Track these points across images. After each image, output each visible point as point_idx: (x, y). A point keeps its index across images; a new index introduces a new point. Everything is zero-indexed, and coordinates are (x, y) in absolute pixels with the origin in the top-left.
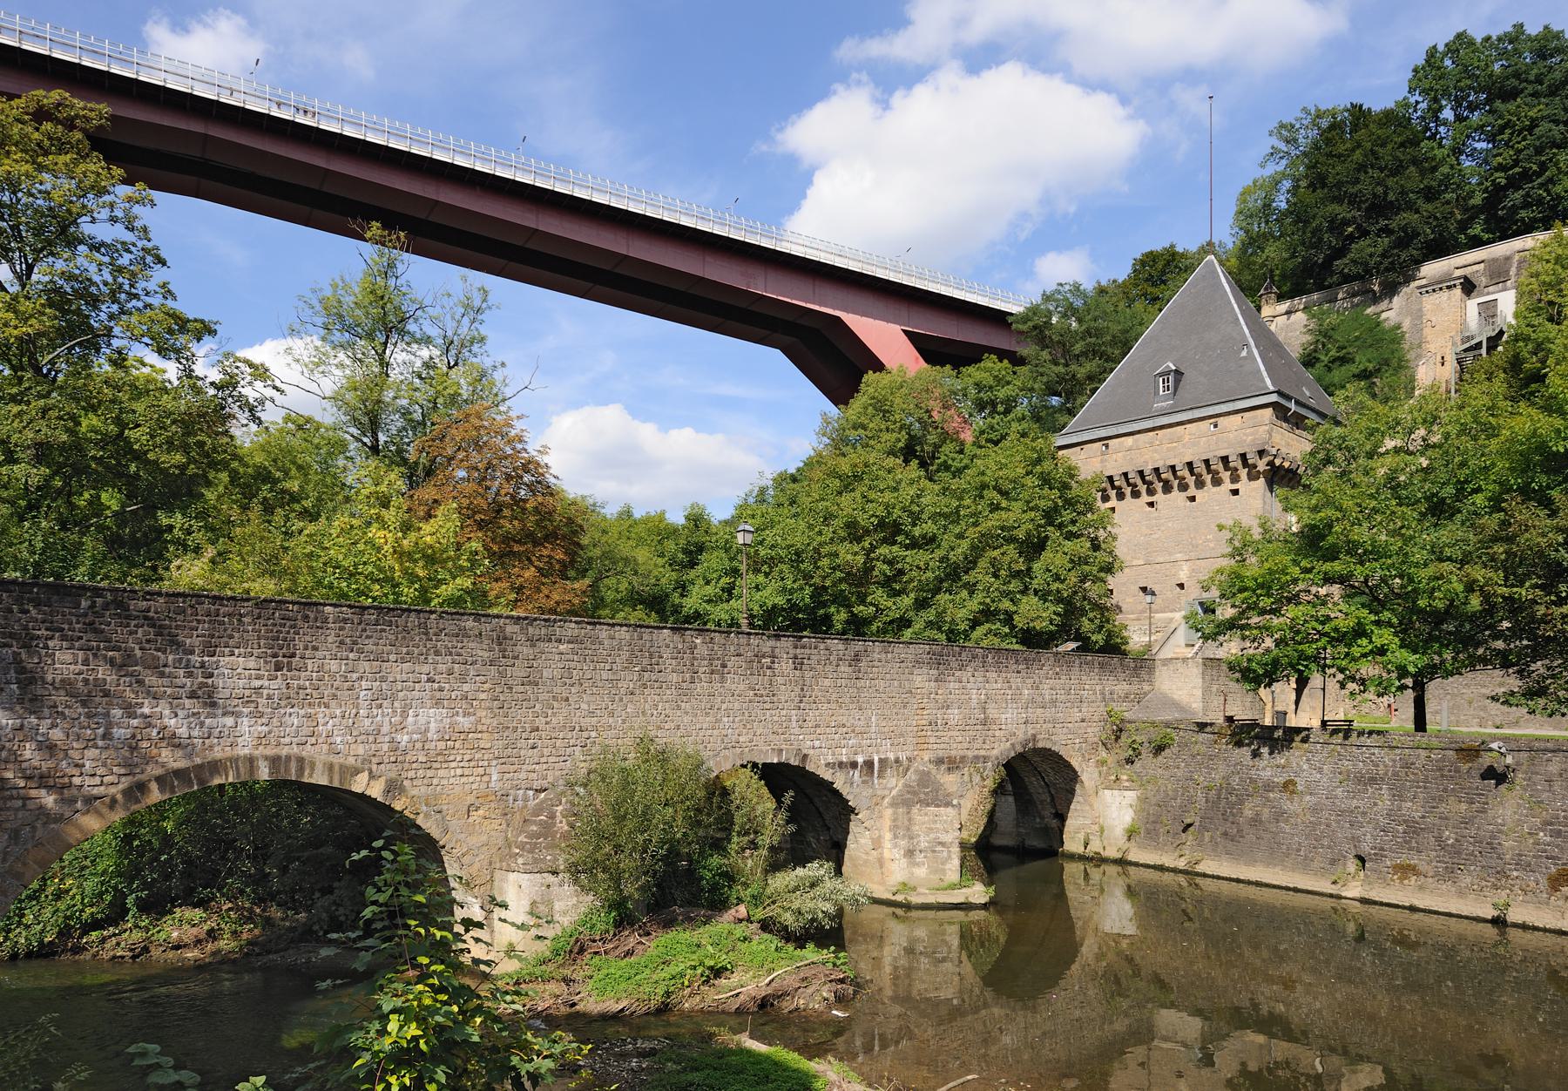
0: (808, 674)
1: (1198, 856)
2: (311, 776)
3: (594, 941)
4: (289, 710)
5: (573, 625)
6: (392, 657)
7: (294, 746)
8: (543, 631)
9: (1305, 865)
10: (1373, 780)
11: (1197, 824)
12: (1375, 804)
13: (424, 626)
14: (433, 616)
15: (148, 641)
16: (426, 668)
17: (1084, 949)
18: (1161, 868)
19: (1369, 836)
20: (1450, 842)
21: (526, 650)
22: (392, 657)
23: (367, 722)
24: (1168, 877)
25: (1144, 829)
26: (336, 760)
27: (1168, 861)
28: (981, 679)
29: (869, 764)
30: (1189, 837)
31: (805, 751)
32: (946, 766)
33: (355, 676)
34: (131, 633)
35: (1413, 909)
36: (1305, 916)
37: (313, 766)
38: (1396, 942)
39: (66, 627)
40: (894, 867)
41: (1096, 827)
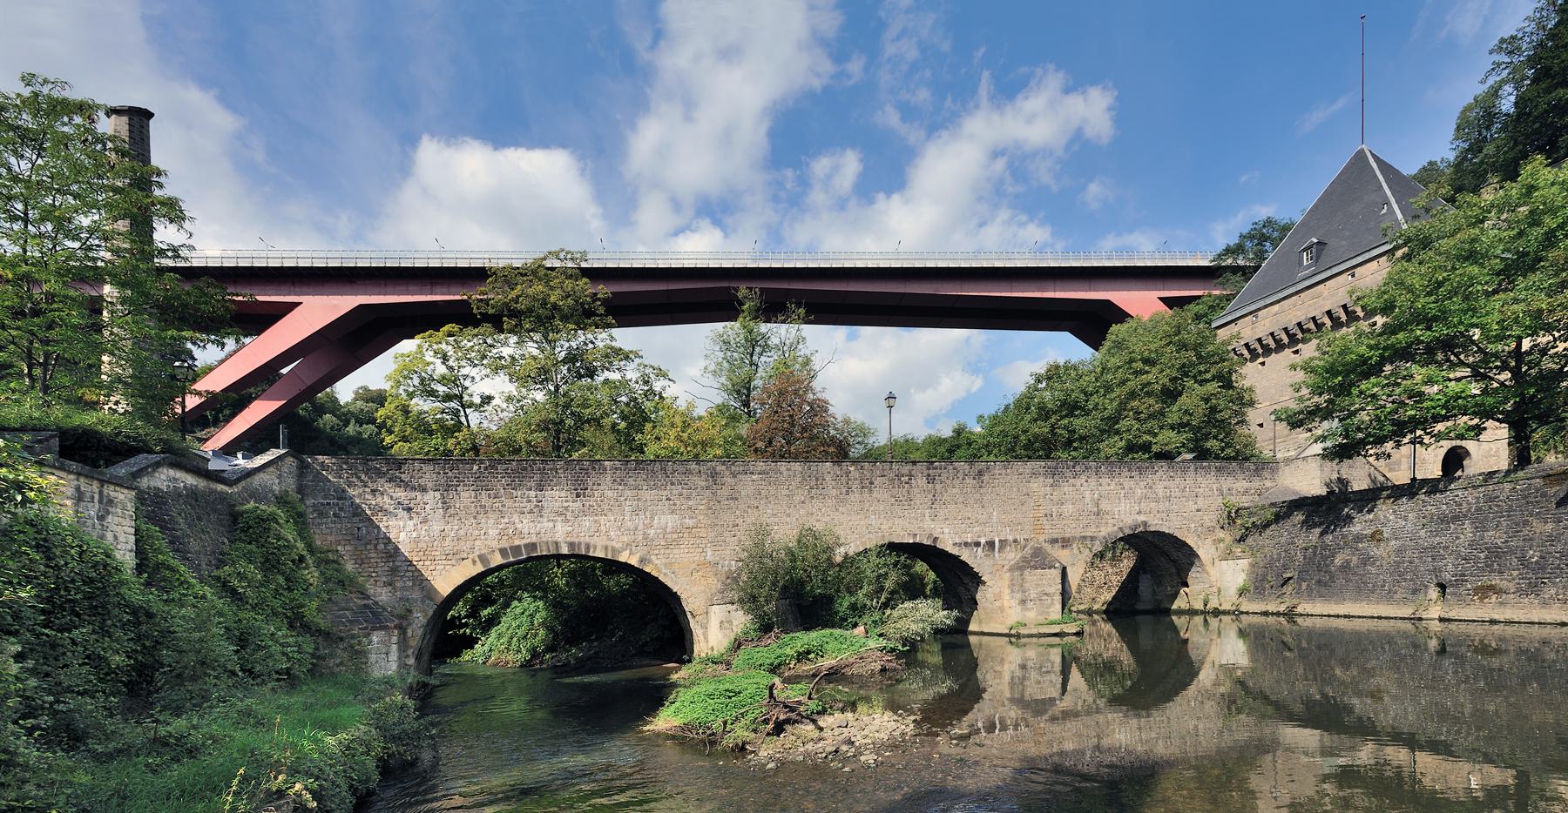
0: (938, 487)
1: (1295, 601)
2: (594, 552)
3: (747, 641)
4: (584, 518)
5: (762, 464)
6: (645, 488)
7: (587, 537)
8: (741, 468)
9: (1389, 597)
10: (1455, 518)
11: (1295, 577)
12: (1458, 538)
13: (664, 469)
14: (670, 463)
15: (508, 485)
16: (665, 493)
17: (1202, 675)
18: (1266, 614)
19: (1450, 566)
20: (1533, 560)
21: (730, 480)
22: (645, 488)
23: (629, 523)
24: (1271, 620)
25: (1257, 586)
26: (610, 544)
27: (1271, 608)
28: (1094, 483)
29: (991, 544)
30: (1288, 589)
31: (936, 535)
32: (1060, 544)
33: (622, 499)
34: (499, 481)
35: (1493, 622)
36: (1388, 639)
37: (595, 548)
38: (1476, 650)
39: (466, 480)
40: (1011, 612)
41: (1215, 589)
